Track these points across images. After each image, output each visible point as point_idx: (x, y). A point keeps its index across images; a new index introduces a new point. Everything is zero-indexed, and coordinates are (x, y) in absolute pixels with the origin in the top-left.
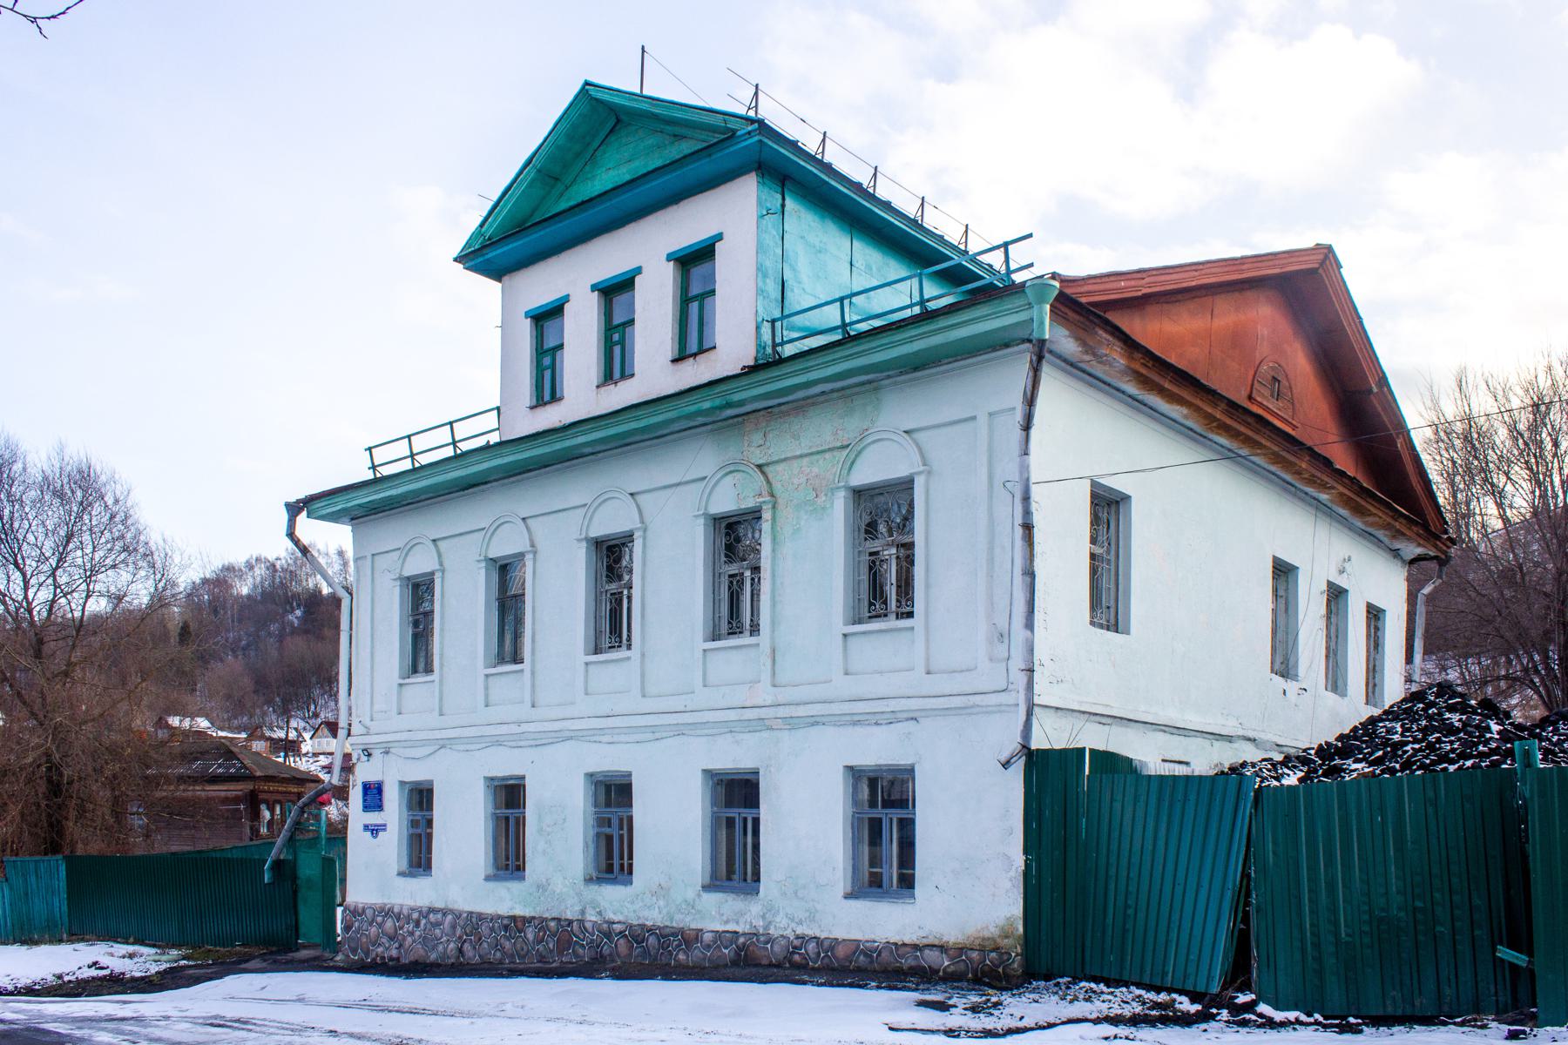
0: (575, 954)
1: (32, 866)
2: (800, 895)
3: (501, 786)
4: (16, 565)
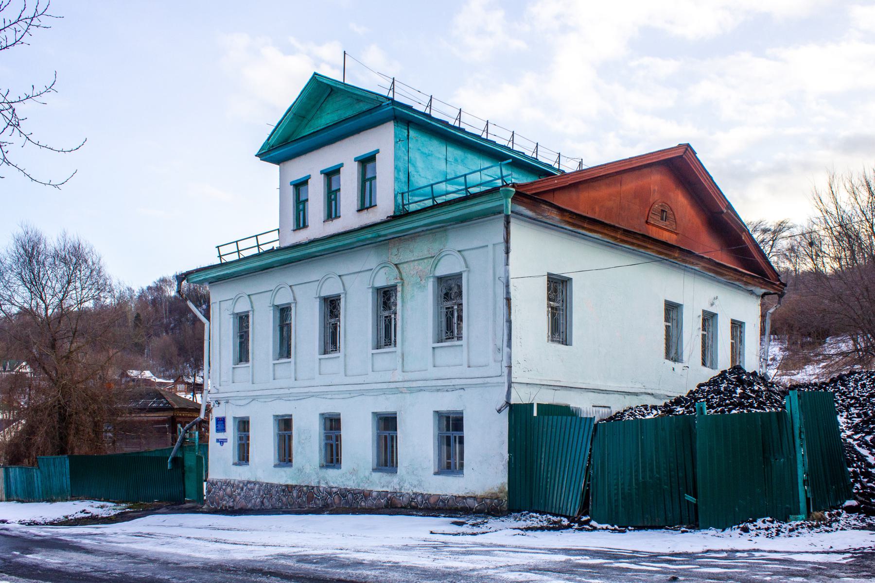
0: (315, 503)
1: (52, 461)
2: (415, 473)
3: (282, 420)
4: (41, 298)
